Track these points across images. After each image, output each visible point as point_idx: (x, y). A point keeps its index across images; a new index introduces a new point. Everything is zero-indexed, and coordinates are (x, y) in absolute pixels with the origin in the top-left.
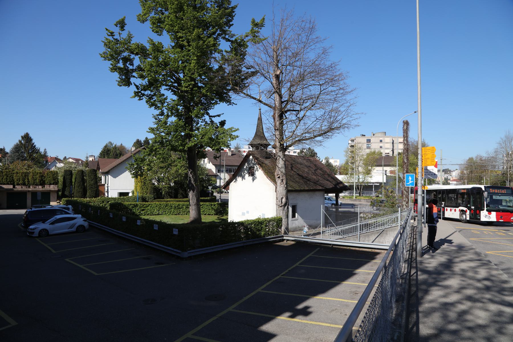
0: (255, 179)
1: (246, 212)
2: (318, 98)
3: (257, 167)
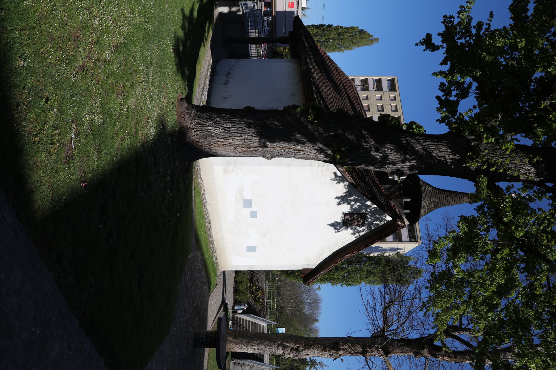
0: (335, 229)
1: (254, 209)
2: (425, 364)
3: (363, 231)
